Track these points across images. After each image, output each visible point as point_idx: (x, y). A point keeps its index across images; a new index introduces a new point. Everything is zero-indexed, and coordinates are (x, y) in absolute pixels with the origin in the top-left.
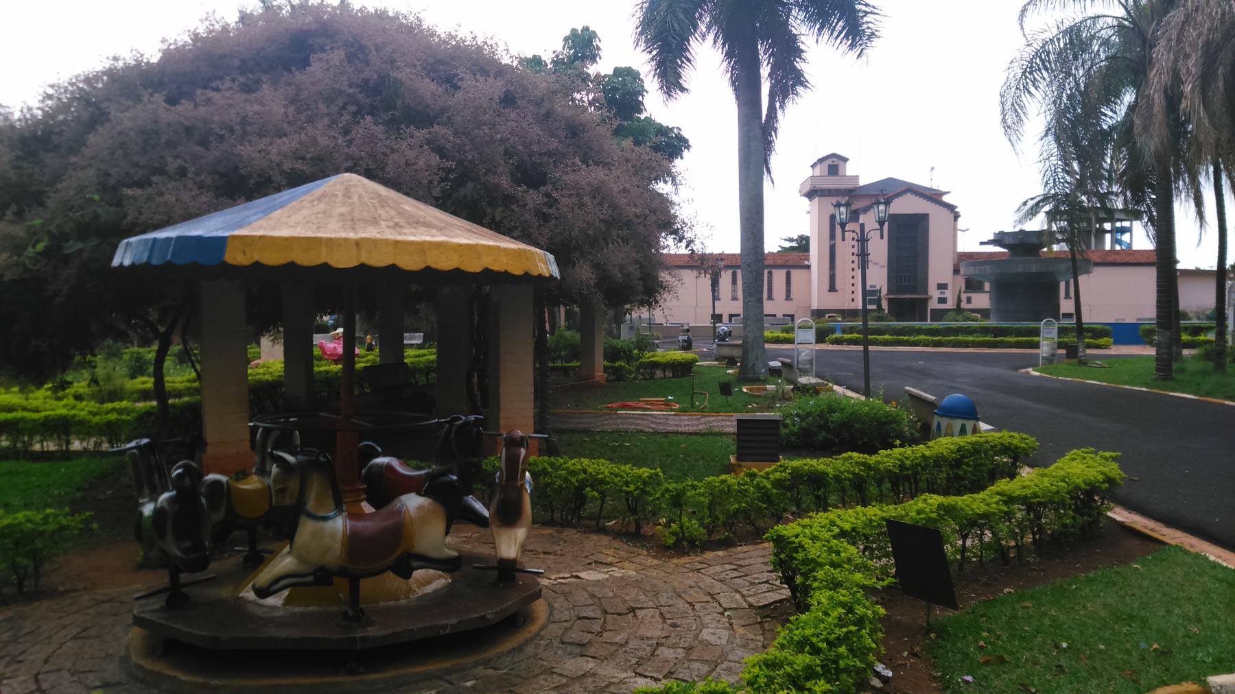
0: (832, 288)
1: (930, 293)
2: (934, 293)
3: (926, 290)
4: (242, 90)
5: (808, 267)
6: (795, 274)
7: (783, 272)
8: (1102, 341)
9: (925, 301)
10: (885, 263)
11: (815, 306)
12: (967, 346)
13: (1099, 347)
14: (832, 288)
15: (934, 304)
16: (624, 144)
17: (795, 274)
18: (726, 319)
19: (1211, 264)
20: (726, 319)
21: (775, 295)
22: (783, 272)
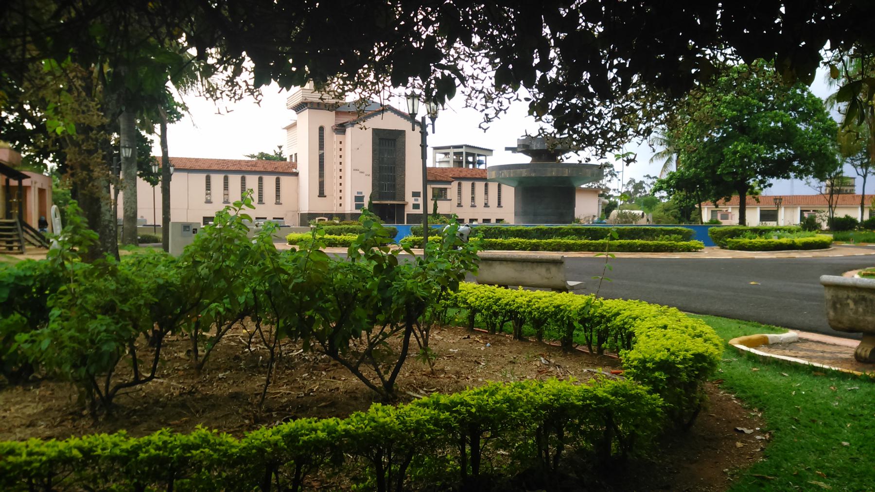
0: (322, 194)
1: (407, 199)
2: (410, 200)
3: (403, 197)
4: (439, 99)
5: (297, 174)
6: (284, 180)
7: (273, 178)
8: (693, 243)
9: (402, 207)
10: (370, 172)
11: (305, 209)
12: (524, 249)
13: (689, 249)
14: (322, 194)
15: (409, 210)
16: (333, 87)
17: (284, 180)
18: (467, 222)
19: (861, 193)
20: (467, 222)
21: (265, 199)
22: (273, 178)
